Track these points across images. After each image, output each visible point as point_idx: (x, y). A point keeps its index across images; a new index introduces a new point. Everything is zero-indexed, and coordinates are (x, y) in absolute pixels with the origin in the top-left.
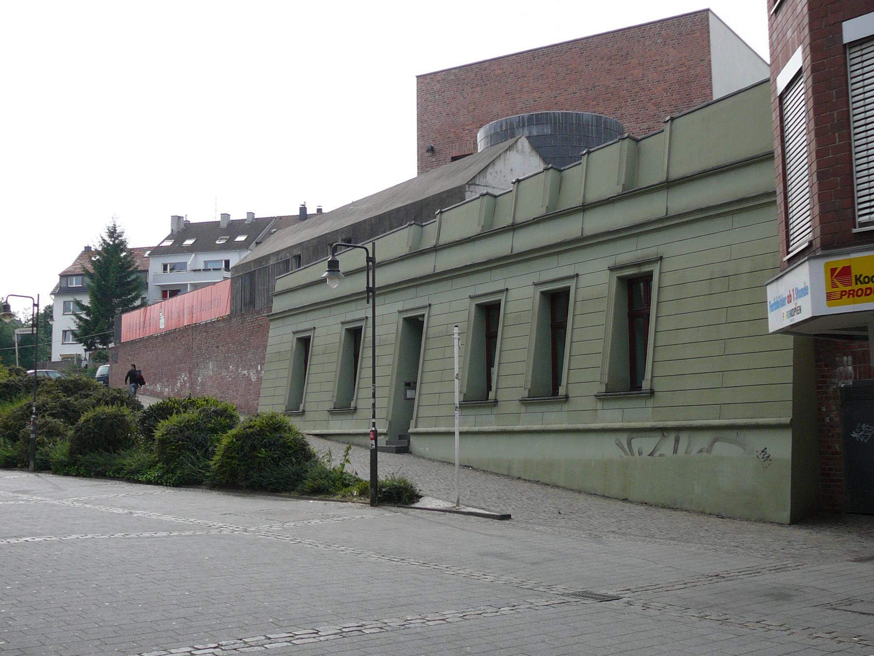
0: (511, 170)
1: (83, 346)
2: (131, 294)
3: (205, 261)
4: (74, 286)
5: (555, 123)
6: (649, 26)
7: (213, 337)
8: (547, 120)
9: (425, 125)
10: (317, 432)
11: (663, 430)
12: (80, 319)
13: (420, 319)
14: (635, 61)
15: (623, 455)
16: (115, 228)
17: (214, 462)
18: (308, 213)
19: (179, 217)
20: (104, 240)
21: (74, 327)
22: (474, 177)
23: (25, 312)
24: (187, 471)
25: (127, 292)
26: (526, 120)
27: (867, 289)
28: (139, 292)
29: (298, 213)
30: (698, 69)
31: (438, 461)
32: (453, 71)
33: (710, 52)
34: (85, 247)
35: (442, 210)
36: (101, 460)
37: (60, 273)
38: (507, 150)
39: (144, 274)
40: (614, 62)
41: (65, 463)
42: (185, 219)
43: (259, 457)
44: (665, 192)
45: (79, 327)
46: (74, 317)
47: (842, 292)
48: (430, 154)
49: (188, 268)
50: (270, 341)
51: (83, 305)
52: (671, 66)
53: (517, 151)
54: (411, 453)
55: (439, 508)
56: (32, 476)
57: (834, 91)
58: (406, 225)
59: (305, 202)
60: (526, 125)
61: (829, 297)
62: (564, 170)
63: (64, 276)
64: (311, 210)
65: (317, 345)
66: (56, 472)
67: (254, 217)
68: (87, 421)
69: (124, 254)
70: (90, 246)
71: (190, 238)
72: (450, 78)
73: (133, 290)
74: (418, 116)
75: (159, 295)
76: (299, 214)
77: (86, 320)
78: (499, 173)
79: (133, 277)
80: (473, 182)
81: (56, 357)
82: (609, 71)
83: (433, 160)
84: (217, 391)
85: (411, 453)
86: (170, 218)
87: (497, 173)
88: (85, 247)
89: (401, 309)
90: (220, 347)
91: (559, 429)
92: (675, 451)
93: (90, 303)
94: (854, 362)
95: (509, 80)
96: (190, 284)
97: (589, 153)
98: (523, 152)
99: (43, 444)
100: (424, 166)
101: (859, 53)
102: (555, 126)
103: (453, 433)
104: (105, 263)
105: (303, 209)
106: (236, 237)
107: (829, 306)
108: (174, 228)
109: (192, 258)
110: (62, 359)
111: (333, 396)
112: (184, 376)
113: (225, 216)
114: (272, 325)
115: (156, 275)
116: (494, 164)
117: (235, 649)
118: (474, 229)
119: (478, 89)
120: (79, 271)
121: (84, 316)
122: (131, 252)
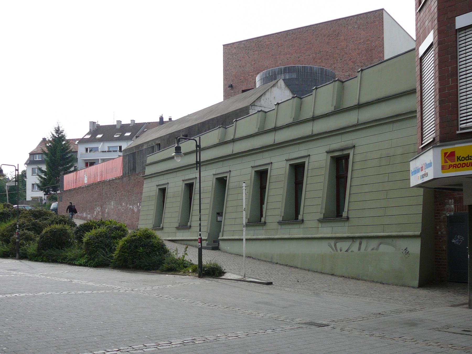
0: (274, 98)
1: (43, 192)
2: (69, 164)
3: (108, 147)
4: (37, 159)
5: (298, 72)
6: (350, 18)
7: (113, 188)
8: (294, 70)
9: (228, 72)
10: (170, 238)
11: (353, 238)
12: (41, 177)
13: (225, 178)
14: (342, 38)
15: (331, 251)
16: (59, 128)
17: (115, 254)
18: (164, 120)
19: (94, 123)
20: (53, 135)
21: (38, 182)
22: (254, 102)
23: (11, 173)
24: (100, 259)
25: (66, 163)
26: (282, 70)
27: (463, 164)
28: (73, 163)
29: (159, 121)
30: (377, 43)
31: (234, 254)
32: (243, 42)
33: (383, 33)
34: (43, 139)
35: (237, 120)
36: (54, 253)
37: (29, 152)
38: (272, 87)
39: (75, 153)
40: (331, 38)
41: (36, 255)
42: (97, 124)
43: (139, 252)
44: (357, 110)
45: (41, 182)
46: (38, 177)
47: (450, 165)
48: (230, 88)
49: (99, 150)
50: (144, 190)
51: (43, 170)
52: (362, 41)
53: (278, 87)
54: (220, 250)
55: (235, 278)
56: (18, 261)
57: (450, 56)
58: (217, 128)
59: (162, 115)
60: (283, 73)
61: (443, 168)
62: (303, 98)
63: (32, 154)
64: (166, 119)
65: (169, 192)
66: (31, 260)
67: (135, 122)
68: (46, 232)
69: (64, 142)
70: (45, 138)
71: (100, 134)
72: (241, 46)
73: (69, 162)
74: (224, 67)
75: (84, 165)
76: (159, 121)
77: (44, 178)
78: (268, 99)
79: (69, 155)
80: (254, 104)
81: (28, 198)
82: (328, 43)
83: (232, 92)
84: (116, 217)
85: (220, 250)
86: (89, 122)
87: (266, 99)
88: (43, 139)
89: (214, 173)
90: (117, 193)
91: (298, 237)
92: (359, 249)
93: (46, 169)
94: (455, 203)
95: (273, 48)
96: (101, 159)
97: (316, 88)
98: (281, 88)
99: (23, 245)
100: (227, 95)
101: (464, 35)
102: (298, 73)
103: (242, 240)
104: (54, 147)
105: (161, 118)
106: (125, 134)
107: (443, 173)
108: (91, 128)
109: (101, 145)
110: (32, 199)
111: (178, 220)
112: (98, 209)
113: (119, 122)
114: (145, 181)
115: (82, 154)
116: (265, 94)
117: (128, 352)
118: (254, 130)
119: (257, 52)
120: (40, 152)
121: (43, 176)
122: (68, 141)
